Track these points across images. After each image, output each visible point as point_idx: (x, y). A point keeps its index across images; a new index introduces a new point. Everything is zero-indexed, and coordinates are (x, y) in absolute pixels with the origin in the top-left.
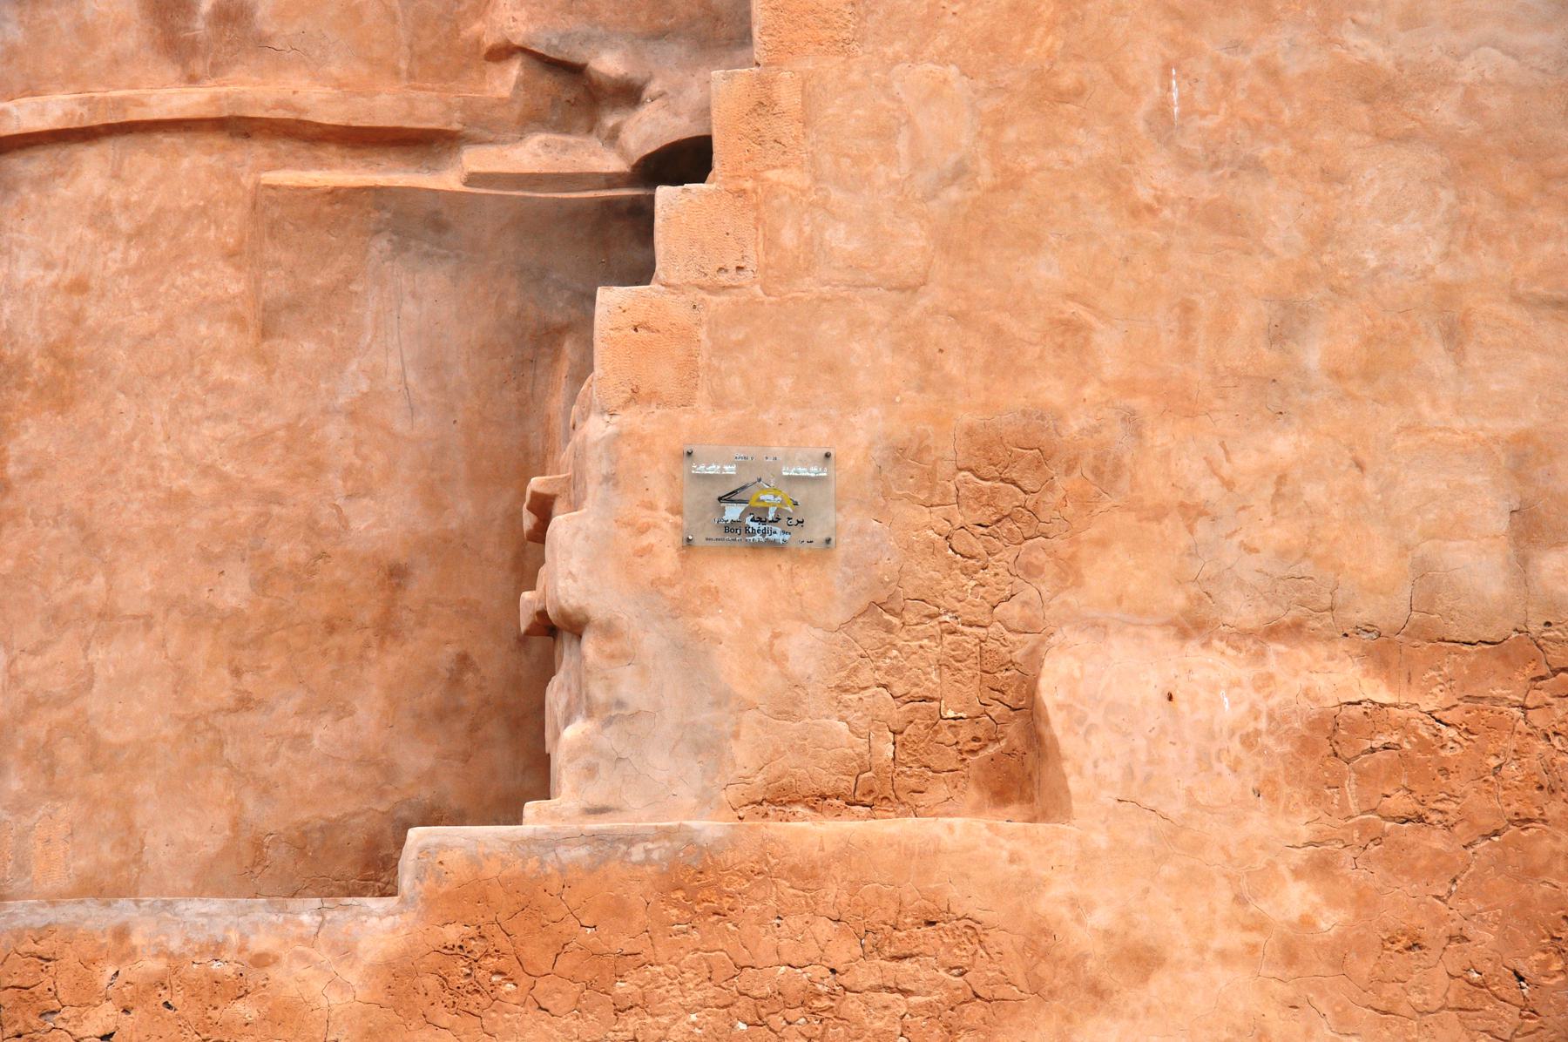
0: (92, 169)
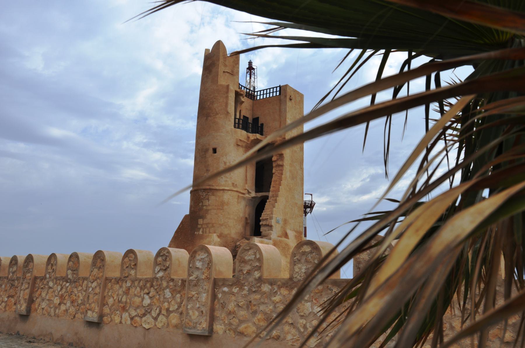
0: (230, 192)
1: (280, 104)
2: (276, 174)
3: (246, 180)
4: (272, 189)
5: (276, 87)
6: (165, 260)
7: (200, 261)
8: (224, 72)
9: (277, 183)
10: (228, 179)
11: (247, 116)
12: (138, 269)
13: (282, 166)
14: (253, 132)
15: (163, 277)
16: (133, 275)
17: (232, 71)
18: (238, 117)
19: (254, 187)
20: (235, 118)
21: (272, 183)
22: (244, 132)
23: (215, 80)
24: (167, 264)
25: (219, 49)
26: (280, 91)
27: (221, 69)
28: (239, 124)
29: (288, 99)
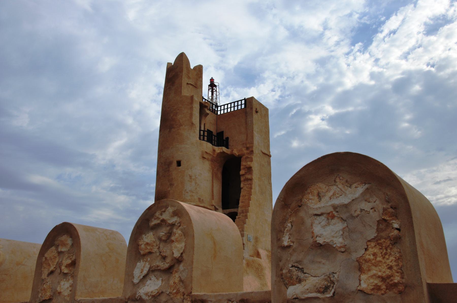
1: (246, 116)
2: (245, 188)
3: (213, 195)
4: (240, 204)
5: (241, 100)
6: (168, 239)
7: (330, 216)
8: (187, 84)
9: (247, 197)
10: (194, 194)
11: (212, 130)
12: (81, 274)
13: (251, 180)
14: (218, 145)
15: (160, 294)
16: (66, 293)
17: (196, 84)
18: (202, 129)
19: (220, 204)
20: (200, 130)
21: (241, 198)
22: (209, 145)
23: (178, 91)
24: (177, 249)
25: (182, 61)
26: (245, 104)
27: (185, 80)
28: (204, 136)
29: (254, 112)
